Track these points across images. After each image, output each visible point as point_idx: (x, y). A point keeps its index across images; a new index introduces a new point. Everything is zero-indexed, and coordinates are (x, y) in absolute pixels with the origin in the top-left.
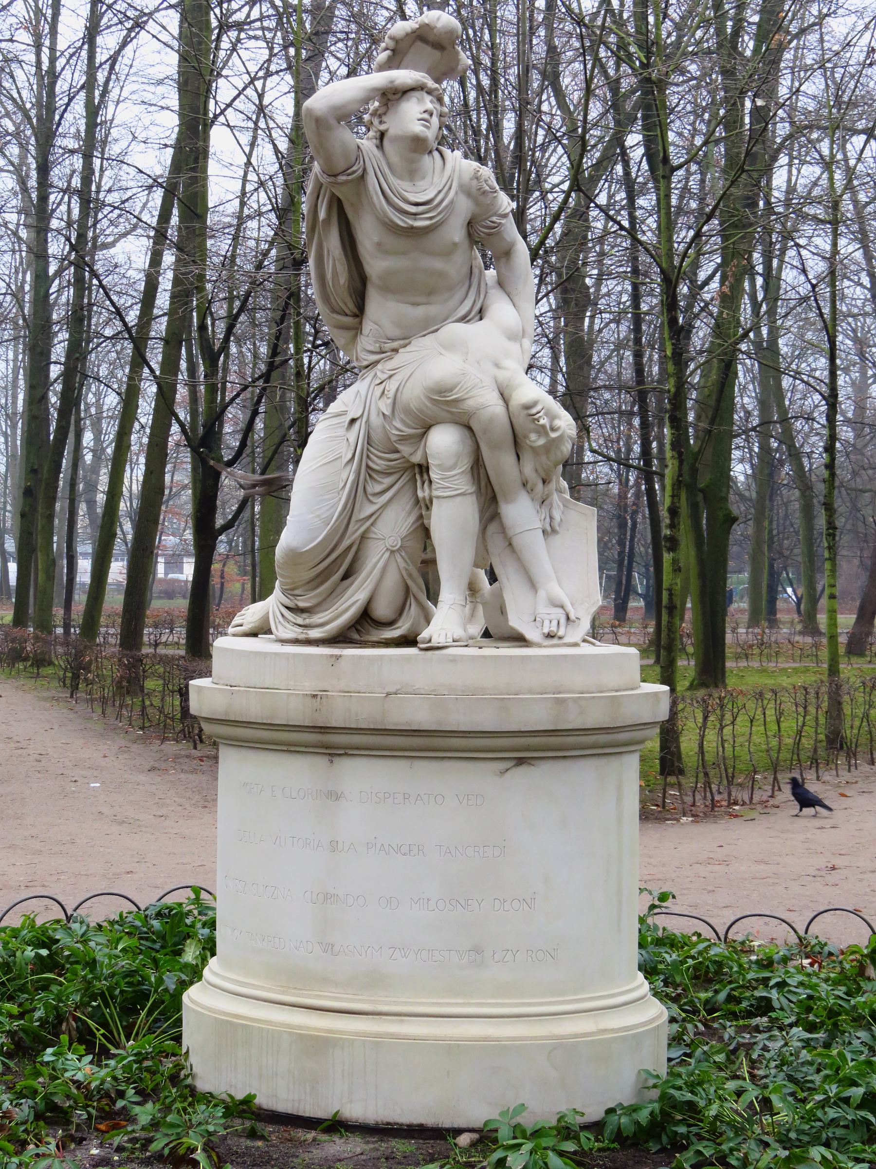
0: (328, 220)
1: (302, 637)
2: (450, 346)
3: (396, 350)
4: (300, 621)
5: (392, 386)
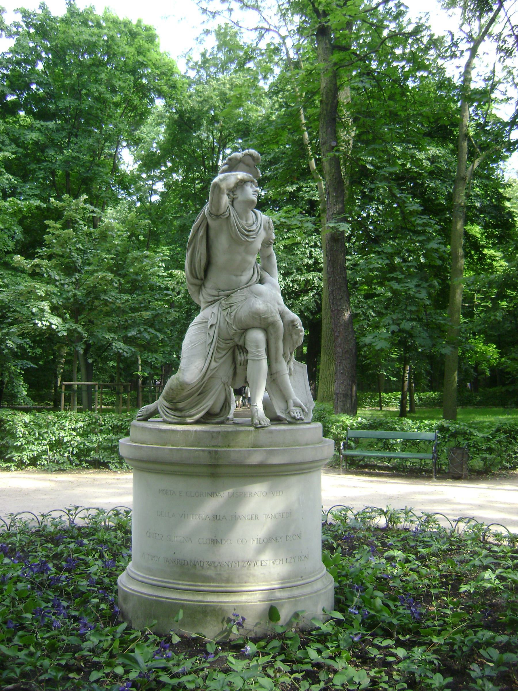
1: (174, 421)
4: (177, 414)
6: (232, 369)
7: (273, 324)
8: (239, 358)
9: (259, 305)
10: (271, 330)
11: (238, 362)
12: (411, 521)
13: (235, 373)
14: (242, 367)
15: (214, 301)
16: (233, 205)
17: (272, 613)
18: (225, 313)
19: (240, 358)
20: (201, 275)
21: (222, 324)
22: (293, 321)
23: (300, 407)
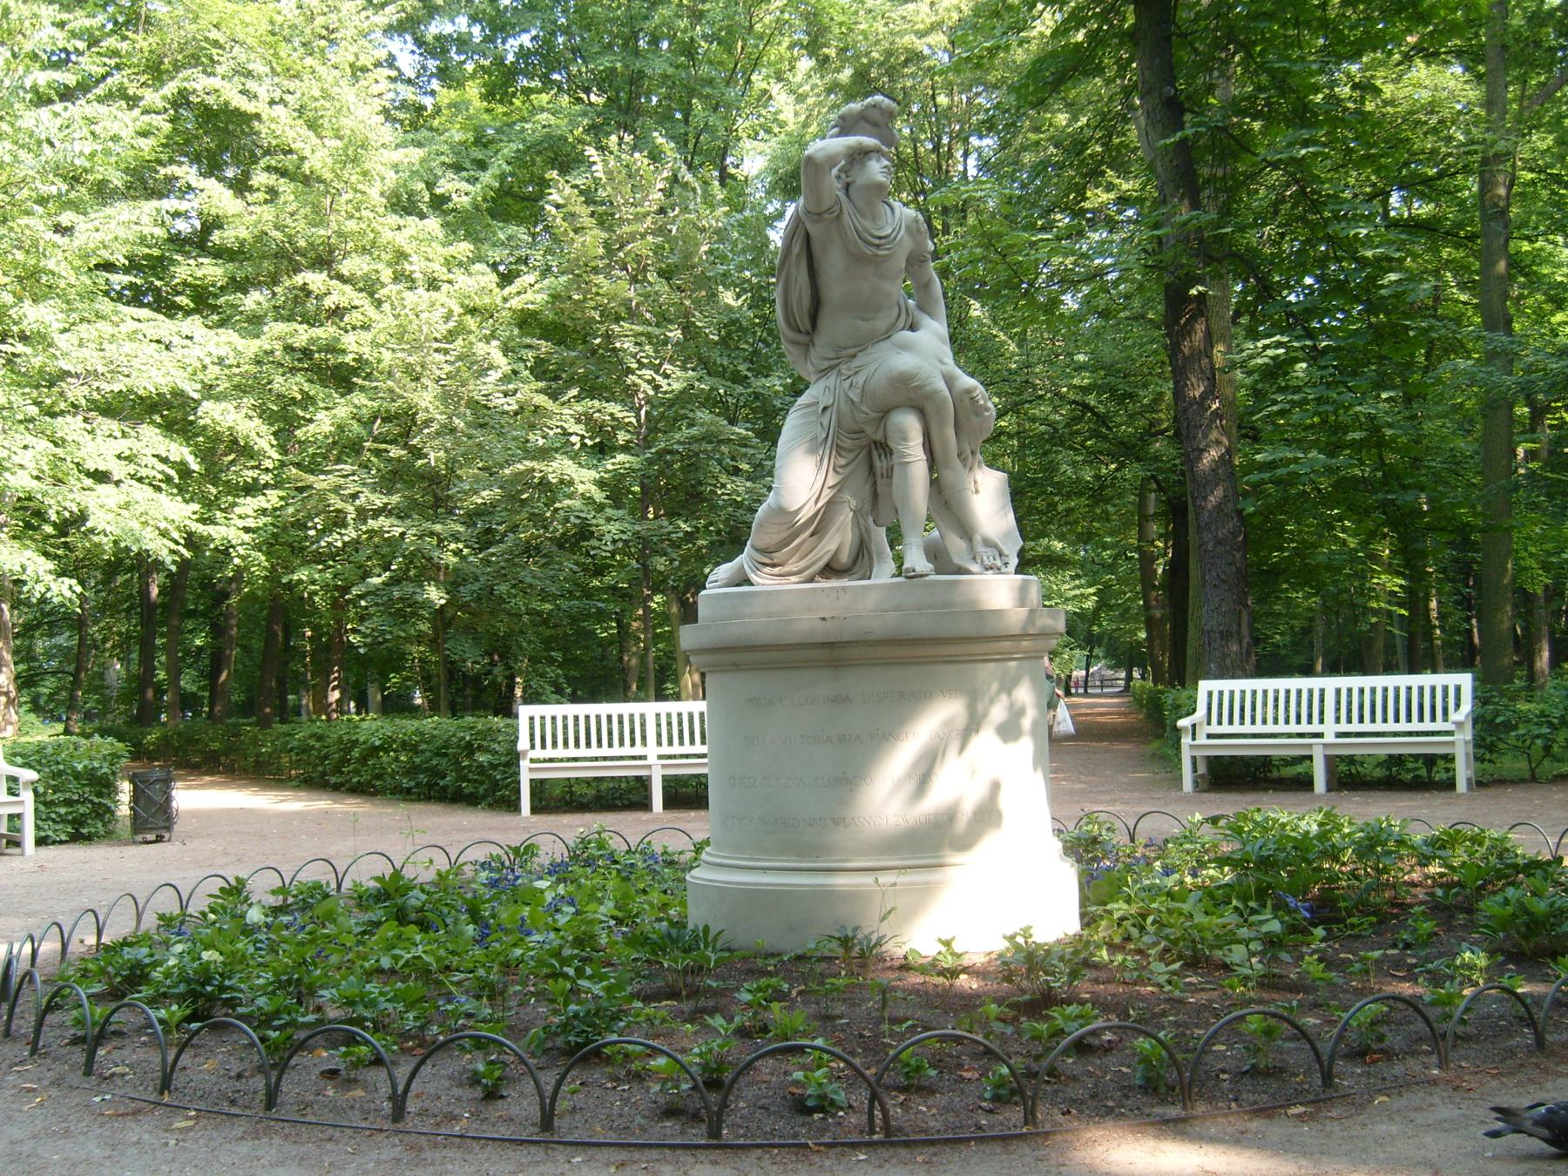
0: (799, 255)
2: (905, 347)
3: (854, 356)
5: (860, 379)
6: (868, 487)
7: (933, 396)
8: (878, 464)
9: (904, 362)
10: (930, 410)
11: (878, 474)
12: (644, 891)
13: (875, 495)
14: (885, 481)
15: (831, 368)
16: (847, 195)
17: (905, 958)
18: (846, 384)
19: (879, 465)
20: (805, 324)
21: (843, 406)
22: (969, 391)
23: (995, 546)
